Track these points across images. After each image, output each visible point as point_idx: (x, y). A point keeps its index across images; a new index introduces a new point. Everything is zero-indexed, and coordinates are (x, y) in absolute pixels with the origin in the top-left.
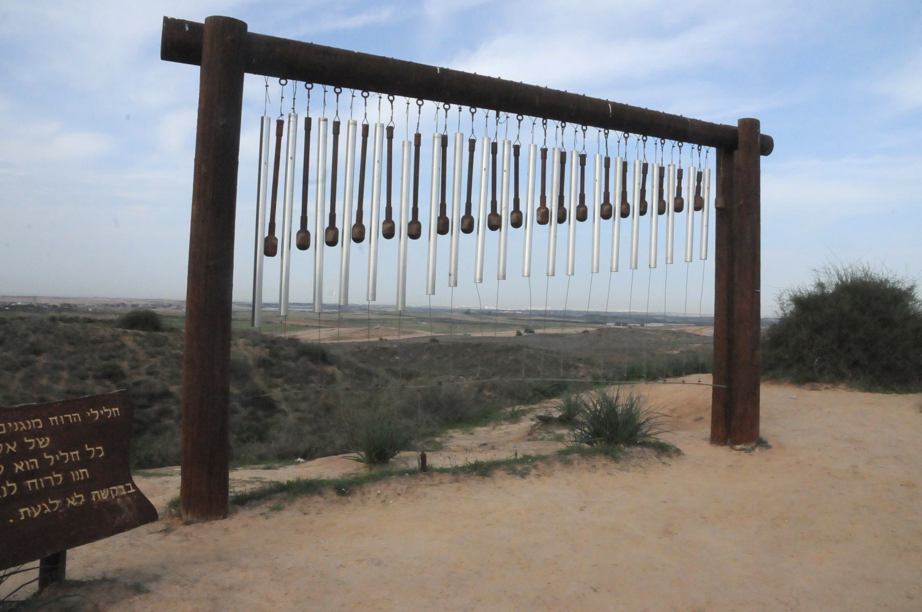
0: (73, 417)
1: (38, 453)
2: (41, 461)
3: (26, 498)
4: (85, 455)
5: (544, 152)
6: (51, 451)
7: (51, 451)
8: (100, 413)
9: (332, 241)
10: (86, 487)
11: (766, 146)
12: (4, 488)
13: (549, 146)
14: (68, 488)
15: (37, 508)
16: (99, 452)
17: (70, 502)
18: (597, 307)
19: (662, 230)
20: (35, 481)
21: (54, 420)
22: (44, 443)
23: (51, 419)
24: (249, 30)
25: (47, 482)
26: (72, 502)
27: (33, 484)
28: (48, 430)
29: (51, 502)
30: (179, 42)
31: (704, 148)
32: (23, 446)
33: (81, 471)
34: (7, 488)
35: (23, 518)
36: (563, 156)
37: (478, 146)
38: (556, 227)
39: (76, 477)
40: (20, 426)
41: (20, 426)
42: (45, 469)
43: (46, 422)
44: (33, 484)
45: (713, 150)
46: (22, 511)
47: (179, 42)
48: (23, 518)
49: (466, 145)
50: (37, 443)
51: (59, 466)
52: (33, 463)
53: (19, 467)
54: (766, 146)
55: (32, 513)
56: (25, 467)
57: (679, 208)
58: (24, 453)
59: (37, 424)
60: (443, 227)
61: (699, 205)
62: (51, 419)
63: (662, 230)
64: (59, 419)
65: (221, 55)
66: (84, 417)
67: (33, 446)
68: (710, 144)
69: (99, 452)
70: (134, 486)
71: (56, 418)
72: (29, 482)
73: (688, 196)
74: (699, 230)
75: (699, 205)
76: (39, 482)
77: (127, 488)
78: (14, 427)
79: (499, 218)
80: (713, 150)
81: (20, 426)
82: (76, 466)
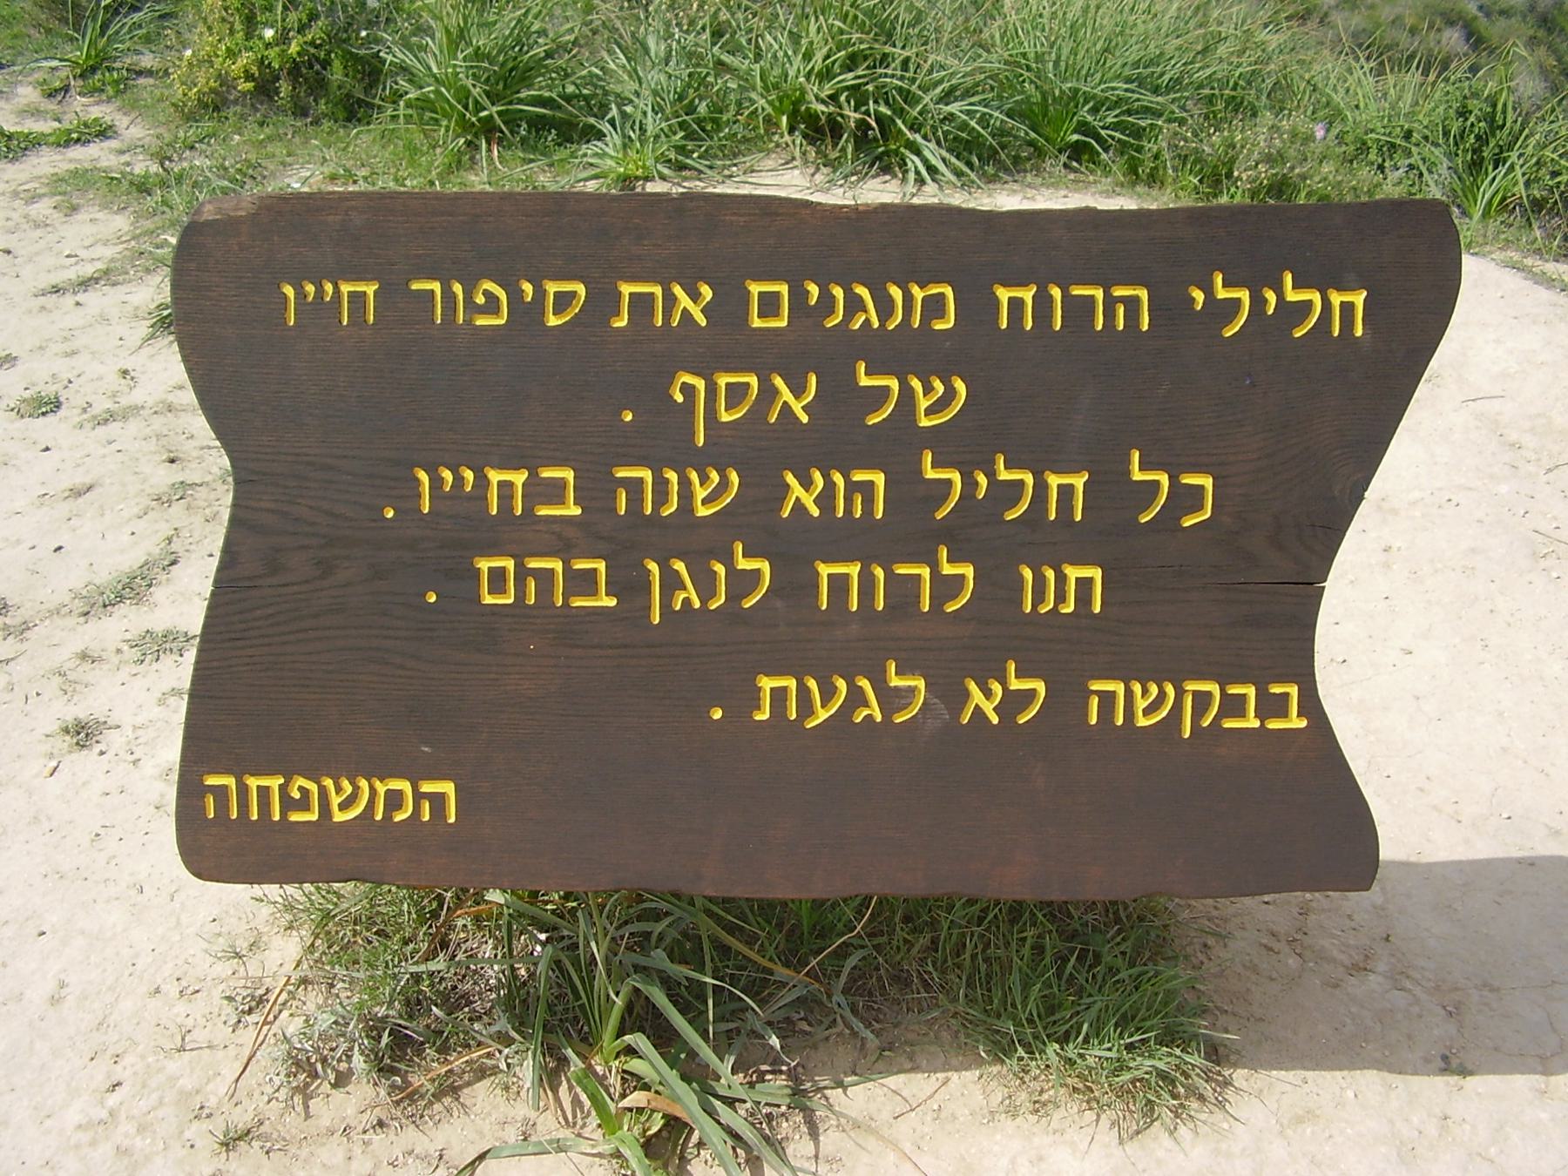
0: (1110, 303)
1: (897, 445)
2: (905, 482)
3: (797, 633)
4: (1111, 489)
6: (960, 445)
7: (960, 445)
8: (1258, 302)
10: (1067, 651)
12: (720, 569)
14: (994, 634)
15: (828, 694)
16: (1187, 499)
17: (977, 696)
20: (854, 570)
21: (1016, 305)
22: (936, 401)
23: (1004, 294)
25: (904, 590)
26: (983, 701)
27: (1016, 305)
28: (974, 349)
29: (895, 681)
32: (841, 399)
33: (1073, 573)
34: (731, 571)
35: (763, 715)
39: (1039, 597)
40: (855, 307)
41: (854, 305)
42: (912, 526)
43: (977, 306)
44: (839, 585)
46: (767, 684)
48: (763, 715)
50: (907, 393)
51: (976, 531)
52: (1132, 304)
53: (801, 495)
55: (806, 708)
56: (826, 499)
58: (837, 438)
59: (934, 307)
62: (1004, 294)
64: (1043, 301)
66: (1169, 307)
67: (1023, 507)
69: (1187, 499)
70: (1311, 705)
71: (1028, 295)
72: (825, 570)
76: (867, 580)
77: (1272, 706)
78: (827, 301)
81: (854, 305)
82: (1051, 540)
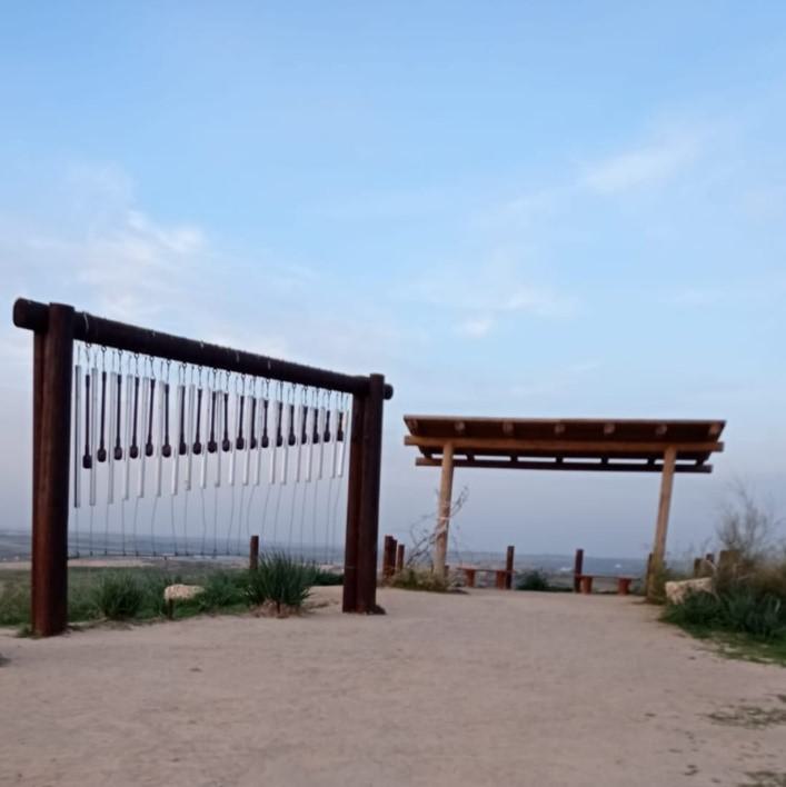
5: (242, 398)
9: (226, 448)
11: (388, 392)
13: (246, 395)
18: (143, 530)
19: (255, 462)
24: (386, 403)
30: (27, 314)
31: (345, 395)
36: (292, 408)
37: (230, 398)
38: (275, 451)
45: (351, 396)
47: (27, 314)
49: (196, 393)
54: (388, 392)
57: (265, 445)
60: (182, 450)
61: (340, 437)
63: (255, 462)
65: (54, 329)
68: (348, 391)
73: (333, 431)
74: (338, 455)
75: (340, 437)
79: (215, 445)
80: (351, 396)
